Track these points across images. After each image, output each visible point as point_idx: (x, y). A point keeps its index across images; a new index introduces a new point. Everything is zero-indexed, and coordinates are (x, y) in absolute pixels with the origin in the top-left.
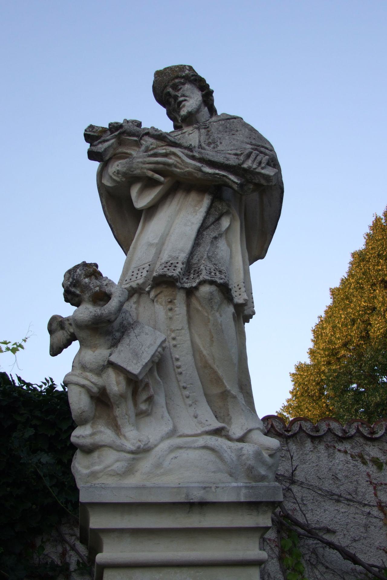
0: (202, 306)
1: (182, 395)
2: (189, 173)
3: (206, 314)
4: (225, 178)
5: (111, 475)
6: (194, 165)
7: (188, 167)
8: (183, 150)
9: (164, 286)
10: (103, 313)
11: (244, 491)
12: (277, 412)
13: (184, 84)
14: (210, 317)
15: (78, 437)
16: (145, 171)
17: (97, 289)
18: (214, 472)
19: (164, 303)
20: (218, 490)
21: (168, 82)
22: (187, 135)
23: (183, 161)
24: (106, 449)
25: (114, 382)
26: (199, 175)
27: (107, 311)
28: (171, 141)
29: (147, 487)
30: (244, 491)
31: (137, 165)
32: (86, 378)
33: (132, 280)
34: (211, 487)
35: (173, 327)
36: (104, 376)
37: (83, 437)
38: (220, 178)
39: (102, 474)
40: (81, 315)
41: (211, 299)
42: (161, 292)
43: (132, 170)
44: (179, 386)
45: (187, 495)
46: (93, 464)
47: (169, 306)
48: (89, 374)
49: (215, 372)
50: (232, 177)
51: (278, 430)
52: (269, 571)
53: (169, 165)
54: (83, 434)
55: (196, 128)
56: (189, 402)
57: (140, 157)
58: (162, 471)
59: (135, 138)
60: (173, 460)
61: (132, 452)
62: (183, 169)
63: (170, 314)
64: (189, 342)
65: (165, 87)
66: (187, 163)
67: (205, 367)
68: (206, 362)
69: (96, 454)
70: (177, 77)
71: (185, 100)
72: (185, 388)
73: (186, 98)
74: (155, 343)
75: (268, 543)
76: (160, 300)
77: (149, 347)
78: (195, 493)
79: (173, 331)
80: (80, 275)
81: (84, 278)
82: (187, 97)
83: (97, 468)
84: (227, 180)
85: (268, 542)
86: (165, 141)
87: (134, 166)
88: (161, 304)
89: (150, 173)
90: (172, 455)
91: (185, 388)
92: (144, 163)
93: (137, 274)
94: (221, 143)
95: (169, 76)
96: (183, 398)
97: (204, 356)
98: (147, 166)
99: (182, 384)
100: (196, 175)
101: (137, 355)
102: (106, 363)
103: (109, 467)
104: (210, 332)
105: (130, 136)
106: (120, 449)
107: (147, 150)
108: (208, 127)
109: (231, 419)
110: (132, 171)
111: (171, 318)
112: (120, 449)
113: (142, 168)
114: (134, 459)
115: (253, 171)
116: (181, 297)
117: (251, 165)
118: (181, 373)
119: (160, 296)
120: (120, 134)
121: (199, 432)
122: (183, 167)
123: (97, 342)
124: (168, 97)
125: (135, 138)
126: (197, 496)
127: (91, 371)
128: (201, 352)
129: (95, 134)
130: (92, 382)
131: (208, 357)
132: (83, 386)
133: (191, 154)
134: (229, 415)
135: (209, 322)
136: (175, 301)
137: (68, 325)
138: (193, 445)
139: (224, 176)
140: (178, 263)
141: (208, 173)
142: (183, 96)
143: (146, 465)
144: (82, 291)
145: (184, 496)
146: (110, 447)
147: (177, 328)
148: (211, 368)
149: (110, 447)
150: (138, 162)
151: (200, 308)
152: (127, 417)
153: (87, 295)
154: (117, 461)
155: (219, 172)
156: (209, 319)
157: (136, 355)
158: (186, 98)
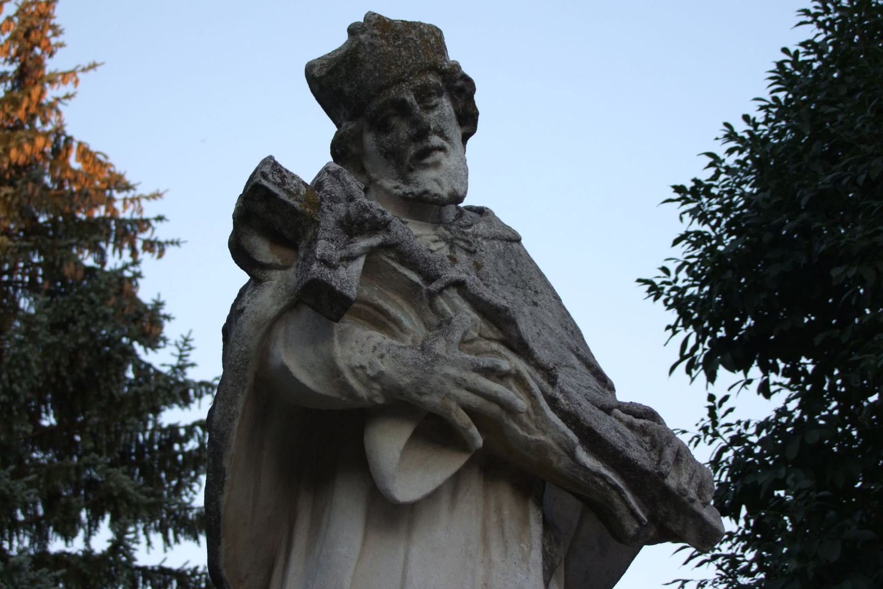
2: (541, 448)
4: (614, 493)
6: (564, 433)
7: (544, 433)
12: (108, 541)
16: (453, 405)
21: (411, 74)
26: (562, 463)
31: (442, 383)
43: (424, 390)
55: (445, 240)
57: (453, 363)
59: (415, 277)
62: (529, 430)
65: (398, 81)
66: (547, 420)
71: (442, 149)
73: (446, 145)
82: (447, 139)
84: (617, 501)
86: (500, 329)
87: (433, 381)
89: (462, 419)
92: (459, 383)
98: (464, 394)
100: (554, 459)
105: (402, 263)
110: (421, 394)
113: (448, 395)
115: (684, 503)
117: (686, 486)
122: (532, 426)
124: (391, 111)
125: (415, 277)
129: (291, 201)
133: (550, 390)
139: (615, 487)
141: (583, 467)
150: (446, 376)
155: (614, 479)
158: (446, 145)
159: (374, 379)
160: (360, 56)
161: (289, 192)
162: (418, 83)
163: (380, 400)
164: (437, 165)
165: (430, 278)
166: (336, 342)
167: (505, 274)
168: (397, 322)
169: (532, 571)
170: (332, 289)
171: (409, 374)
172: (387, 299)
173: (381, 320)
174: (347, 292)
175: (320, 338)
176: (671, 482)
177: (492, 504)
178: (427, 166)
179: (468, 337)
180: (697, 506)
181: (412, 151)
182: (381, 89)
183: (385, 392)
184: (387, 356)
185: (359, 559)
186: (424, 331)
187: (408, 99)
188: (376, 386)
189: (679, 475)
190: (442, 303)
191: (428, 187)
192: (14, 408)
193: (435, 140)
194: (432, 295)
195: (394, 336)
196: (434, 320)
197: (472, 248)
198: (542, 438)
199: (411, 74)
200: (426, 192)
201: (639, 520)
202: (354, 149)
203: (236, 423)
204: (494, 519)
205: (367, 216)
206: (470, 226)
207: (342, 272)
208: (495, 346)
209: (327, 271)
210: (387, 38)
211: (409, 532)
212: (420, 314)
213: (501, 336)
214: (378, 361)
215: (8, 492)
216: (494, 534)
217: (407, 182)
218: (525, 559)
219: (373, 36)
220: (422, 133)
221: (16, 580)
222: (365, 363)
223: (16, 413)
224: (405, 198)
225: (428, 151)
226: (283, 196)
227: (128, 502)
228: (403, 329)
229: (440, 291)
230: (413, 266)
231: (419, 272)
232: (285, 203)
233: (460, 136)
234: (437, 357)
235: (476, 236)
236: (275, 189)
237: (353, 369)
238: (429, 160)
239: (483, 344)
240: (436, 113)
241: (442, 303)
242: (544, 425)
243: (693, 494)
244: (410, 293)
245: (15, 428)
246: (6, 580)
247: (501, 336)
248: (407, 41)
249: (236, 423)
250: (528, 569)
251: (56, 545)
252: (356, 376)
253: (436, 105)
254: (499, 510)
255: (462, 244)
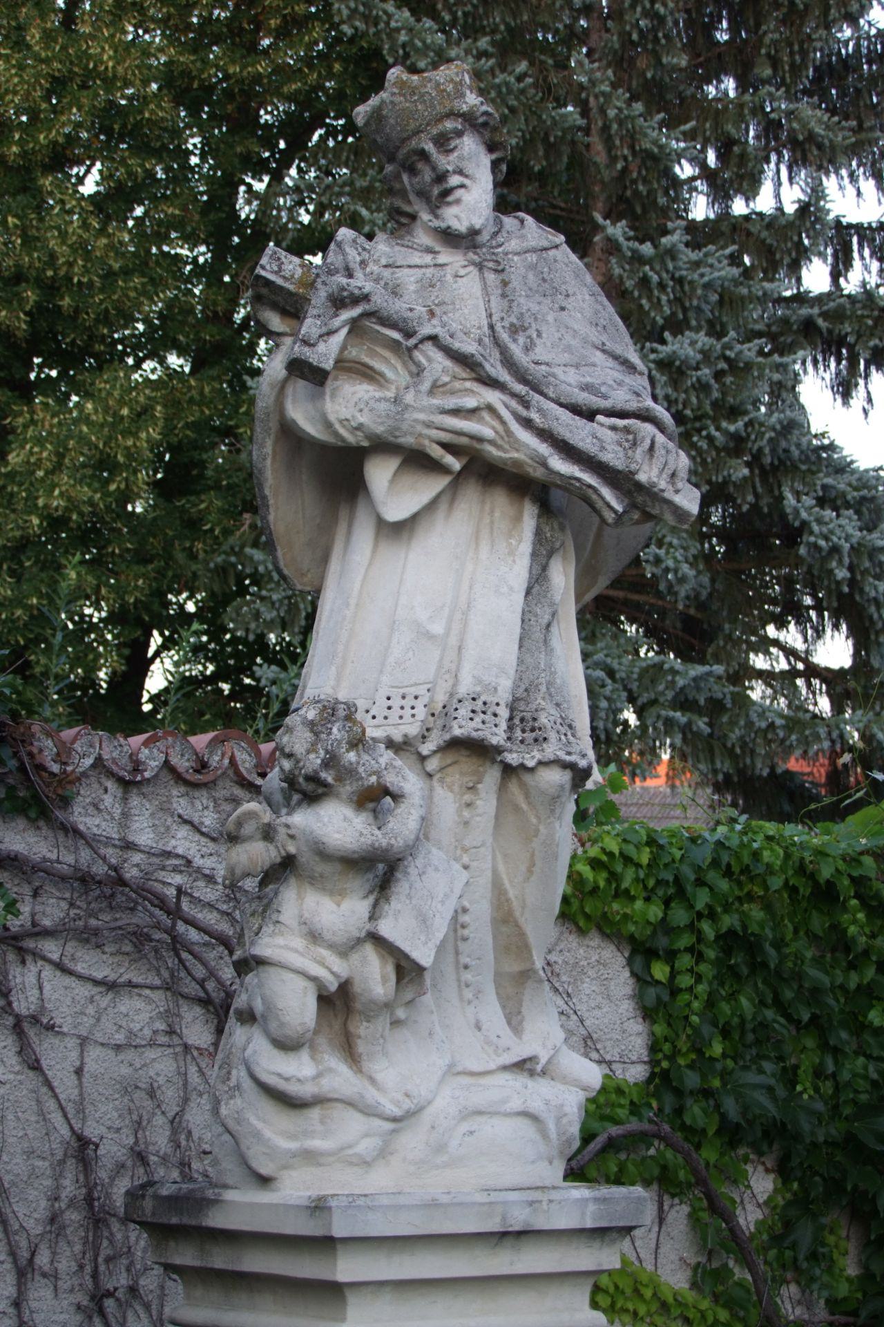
0: (529, 803)
1: (459, 980)
2: (516, 463)
3: (534, 821)
4: (590, 491)
5: (351, 1164)
7: (517, 450)
8: (506, 398)
9: (464, 752)
10: (392, 846)
11: (592, 1207)
13: (460, 134)
14: (542, 828)
15: (287, 1079)
16: (426, 442)
17: (373, 779)
18: (533, 1162)
19: (456, 788)
20: (552, 1206)
21: (428, 125)
22: (449, 278)
23: (509, 433)
24: (339, 1105)
25: (379, 977)
26: (539, 473)
27: (401, 843)
28: (489, 376)
29: (441, 1205)
30: (592, 1207)
32: (322, 963)
33: (389, 721)
34: (541, 1202)
35: (467, 843)
36: (355, 957)
37: (299, 1080)
38: (580, 489)
39: (331, 1159)
40: (337, 836)
41: (558, 797)
42: (455, 763)
43: (397, 434)
44: (457, 962)
45: (504, 1218)
46: (308, 1134)
47: (467, 797)
48: (325, 953)
49: (522, 935)
50: (607, 493)
51: (245, 773)
52: (191, 1126)
53: (480, 440)
54: (300, 1075)
55: (474, 263)
56: (468, 994)
57: (422, 410)
58: (445, 1158)
60: (466, 1139)
61: (395, 1120)
63: (466, 814)
64: (489, 874)
65: (417, 132)
66: (517, 441)
67: (505, 921)
68: (510, 913)
69: (315, 1113)
70: (452, 114)
71: (462, 186)
72: (466, 967)
73: (466, 181)
74: (452, 891)
75: (194, 1058)
76: (448, 780)
77: (443, 902)
78: (516, 1213)
79: (465, 850)
80: (339, 742)
81: (348, 751)
82: (467, 176)
83: (317, 1143)
84: (594, 497)
85: (195, 1053)
86: (472, 370)
87: (405, 427)
88: (451, 789)
89: (436, 452)
90: (465, 1127)
91: (466, 967)
92: (429, 425)
93: (402, 708)
94: (539, 335)
95: (433, 106)
96: (459, 986)
97: (508, 900)
98: (435, 433)
99: (464, 960)
100: (530, 470)
101: (424, 921)
102: (363, 934)
103: (350, 1147)
104: (533, 855)
105: (384, 325)
106: (369, 1111)
107: (435, 388)
108: (503, 270)
109: (521, 1022)
110: (396, 437)
111: (466, 823)
112: (369, 1111)
113: (420, 435)
114: (394, 1131)
115: (656, 494)
116: (492, 776)
117: (655, 480)
118: (465, 939)
119: (450, 770)
120: (362, 315)
121: (493, 1066)
122: (507, 447)
123: (348, 885)
124: (415, 158)
125: (396, 335)
126: (519, 1218)
127: (331, 947)
128: (505, 892)
129: (287, 285)
130: (333, 973)
131: (515, 904)
132: (314, 979)
133: (524, 413)
134: (520, 1012)
135: (536, 836)
136: (479, 786)
137: (285, 837)
138: (502, 1110)
139: (590, 486)
140: (498, 704)
142: (460, 172)
143: (413, 1142)
144: (339, 779)
145: (498, 1220)
146: (349, 1103)
147: (475, 844)
148: (517, 926)
149: (349, 1103)
150: (416, 421)
151: (524, 806)
152: (381, 1041)
153: (348, 788)
154: (367, 1135)
156: (537, 831)
157: (424, 921)
158: (466, 181)
159: (357, 429)
160: (384, 113)
161: (284, 277)
162: (435, 131)
163: (365, 444)
164: (458, 201)
165: (409, 335)
166: (328, 398)
167: (534, 286)
168: (382, 375)
169: (518, 561)
170: (310, 365)
171: (382, 423)
172: (373, 354)
173: (368, 374)
174: (323, 365)
175: (317, 397)
176: (642, 477)
177: (487, 507)
178: (449, 204)
179: (440, 383)
180: (669, 495)
181: (436, 191)
182: (404, 141)
183: (367, 437)
184: (366, 410)
185: (370, 564)
186: (408, 378)
187: (426, 148)
188: (359, 433)
189: (651, 469)
190: (418, 355)
191: (450, 224)
192: (660, 35)
193: (454, 180)
194: (409, 350)
195: (381, 386)
196: (414, 369)
197: (500, 268)
198: (516, 455)
199: (428, 125)
200: (449, 227)
201: (615, 512)
202: (397, 186)
203: (269, 462)
204: (487, 520)
205: (345, 294)
206: (500, 246)
207: (321, 347)
208: (468, 384)
209: (306, 349)
210: (404, 95)
211: (410, 538)
212: (404, 364)
213: (474, 375)
214: (358, 415)
215: (656, 150)
216: (485, 534)
217: (437, 217)
218: (512, 553)
219: (393, 94)
220: (441, 177)
221: (671, 266)
222: (349, 417)
223: (663, 41)
224: (435, 229)
225: (447, 192)
226: (280, 281)
227: (820, 147)
228: (387, 381)
229: (416, 346)
230: (394, 326)
231: (400, 330)
232: (281, 288)
233: (489, 165)
234: (407, 407)
235: (507, 254)
236: (272, 277)
237: (341, 421)
238: (450, 199)
239: (457, 385)
240: (456, 154)
241: (418, 355)
242: (516, 444)
243: (663, 484)
244: (395, 346)
245: (664, 60)
246: (658, 268)
247: (474, 375)
248: (422, 96)
249: (269, 462)
250: (514, 561)
251: (739, 207)
252: (344, 426)
253: (456, 147)
254: (492, 511)
255: (491, 265)
